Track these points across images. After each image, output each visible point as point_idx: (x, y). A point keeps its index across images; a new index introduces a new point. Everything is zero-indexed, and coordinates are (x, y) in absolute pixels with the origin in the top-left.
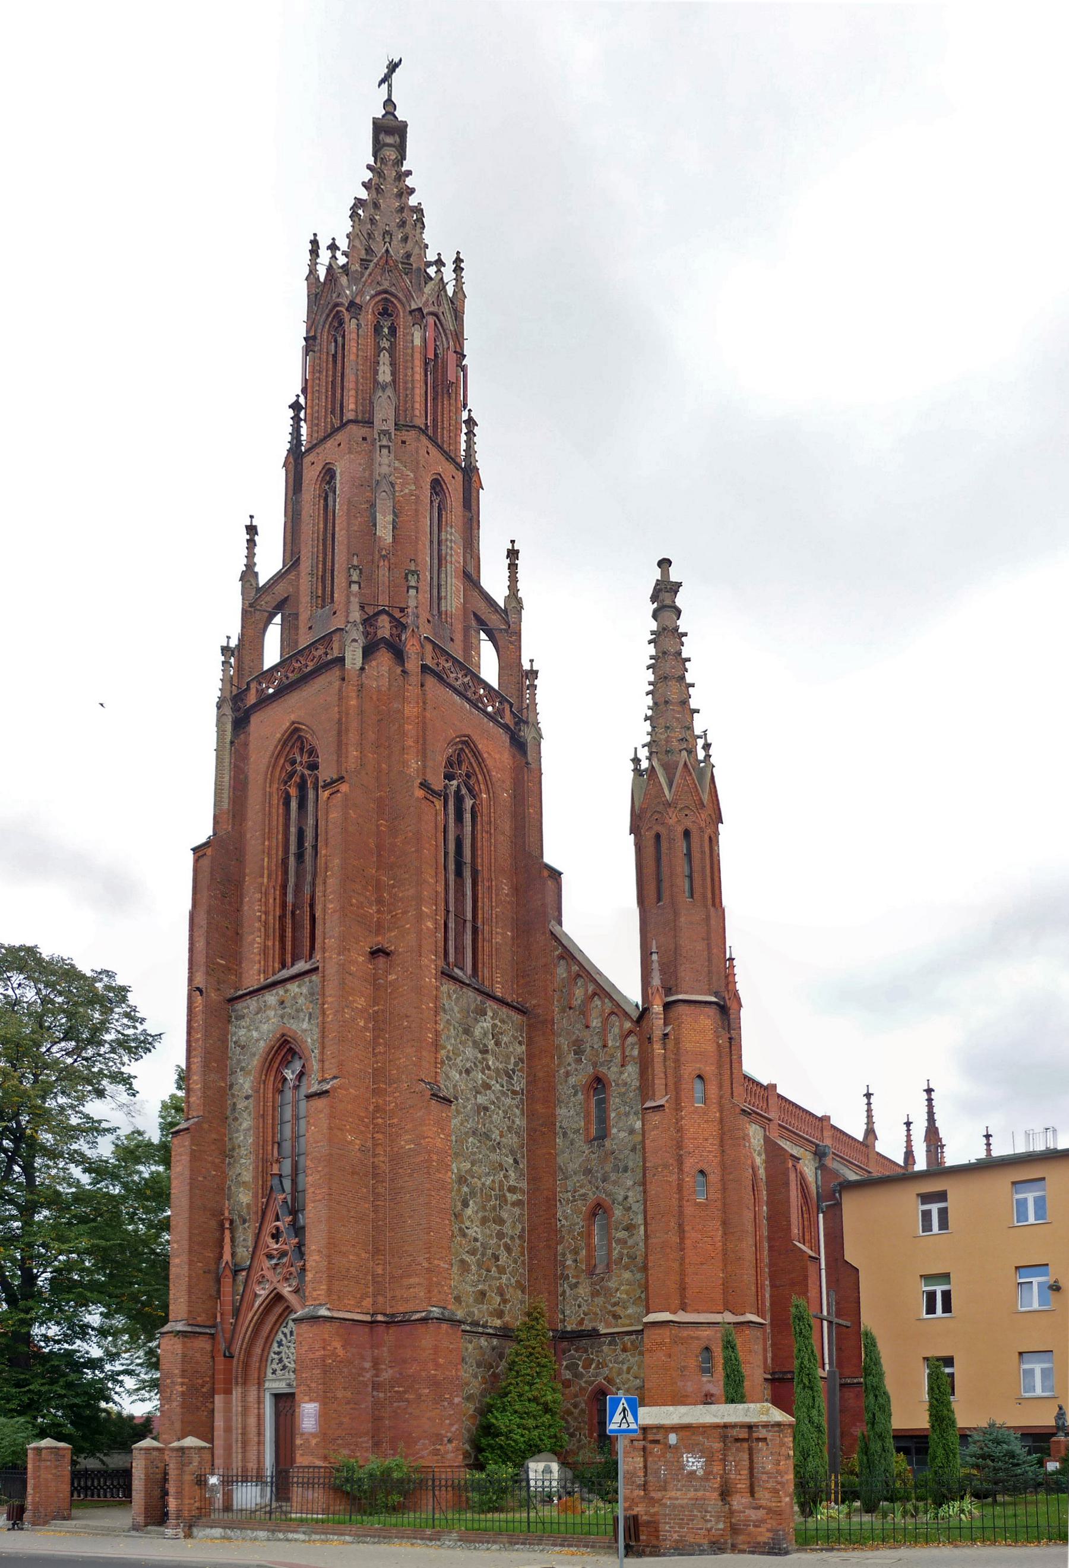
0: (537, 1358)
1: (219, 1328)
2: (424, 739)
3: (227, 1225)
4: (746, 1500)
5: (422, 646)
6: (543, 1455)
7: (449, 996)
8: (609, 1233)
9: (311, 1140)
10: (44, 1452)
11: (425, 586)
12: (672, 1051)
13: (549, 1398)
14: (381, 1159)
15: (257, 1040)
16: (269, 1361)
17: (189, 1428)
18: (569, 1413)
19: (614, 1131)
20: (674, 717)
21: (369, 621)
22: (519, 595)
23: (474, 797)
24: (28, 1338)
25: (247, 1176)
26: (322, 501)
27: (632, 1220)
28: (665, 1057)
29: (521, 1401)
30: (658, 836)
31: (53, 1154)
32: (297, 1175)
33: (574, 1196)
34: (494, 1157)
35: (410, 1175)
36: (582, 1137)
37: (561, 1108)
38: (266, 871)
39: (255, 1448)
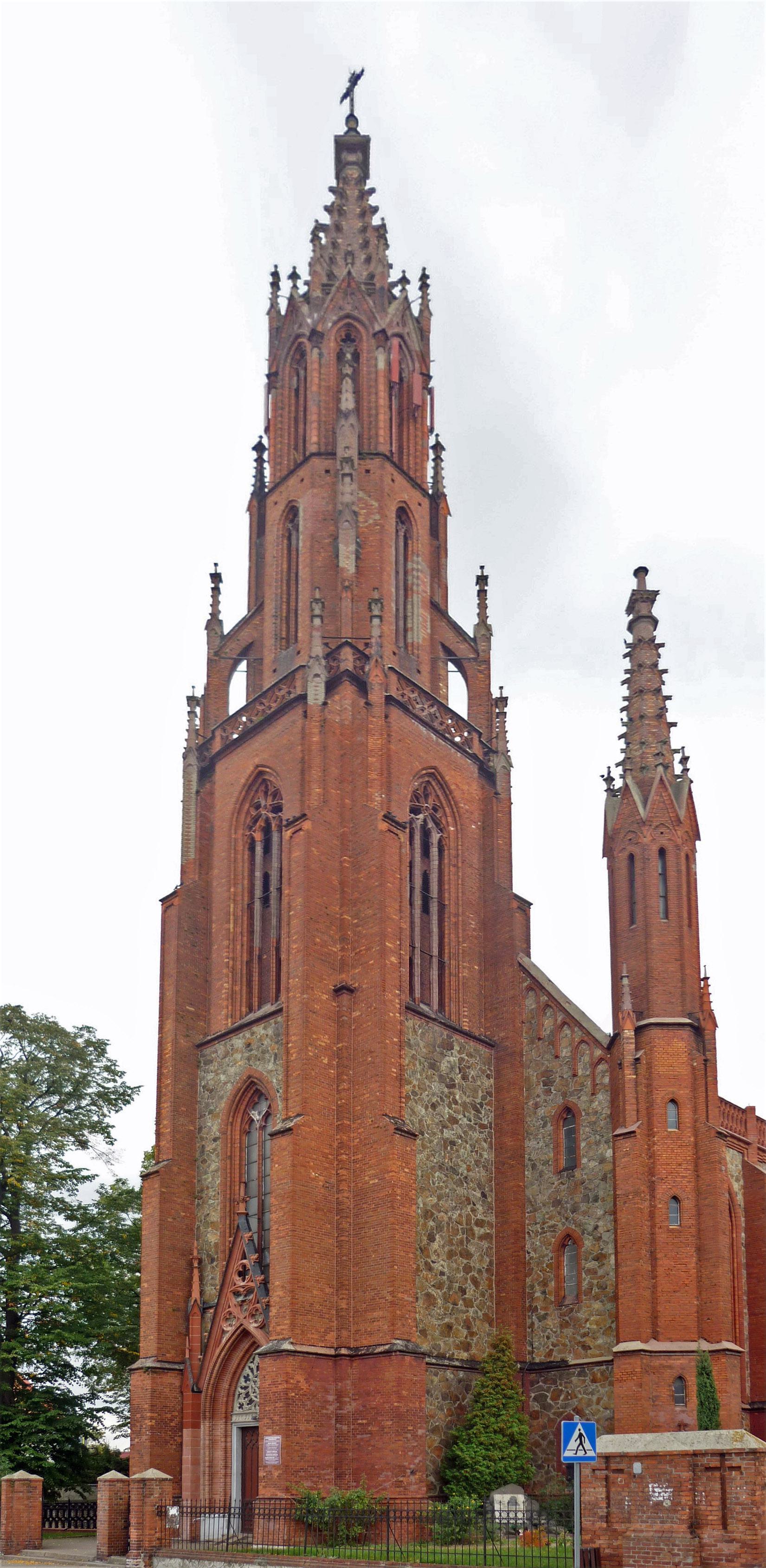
0: (503, 1390)
1: (188, 1363)
2: (389, 773)
3: (196, 1265)
4: (718, 1532)
5: (386, 676)
6: (509, 1487)
7: (415, 1031)
8: (578, 1264)
9: (275, 1178)
10: (17, 1483)
11: (390, 616)
12: (644, 1076)
13: (515, 1429)
14: (346, 1194)
15: (225, 1083)
16: (236, 1396)
17: (157, 1462)
18: (537, 1444)
19: (584, 1161)
20: (650, 732)
21: (331, 655)
22: (489, 622)
23: (441, 830)
24: (13, 1377)
25: (215, 1217)
26: (285, 541)
27: (602, 1249)
28: (636, 1082)
29: (487, 1433)
30: (631, 857)
31: (37, 1202)
32: (263, 1213)
33: (543, 1228)
34: (460, 1191)
35: (375, 1210)
36: (551, 1168)
37: (530, 1140)
38: (232, 917)
39: (222, 1480)
